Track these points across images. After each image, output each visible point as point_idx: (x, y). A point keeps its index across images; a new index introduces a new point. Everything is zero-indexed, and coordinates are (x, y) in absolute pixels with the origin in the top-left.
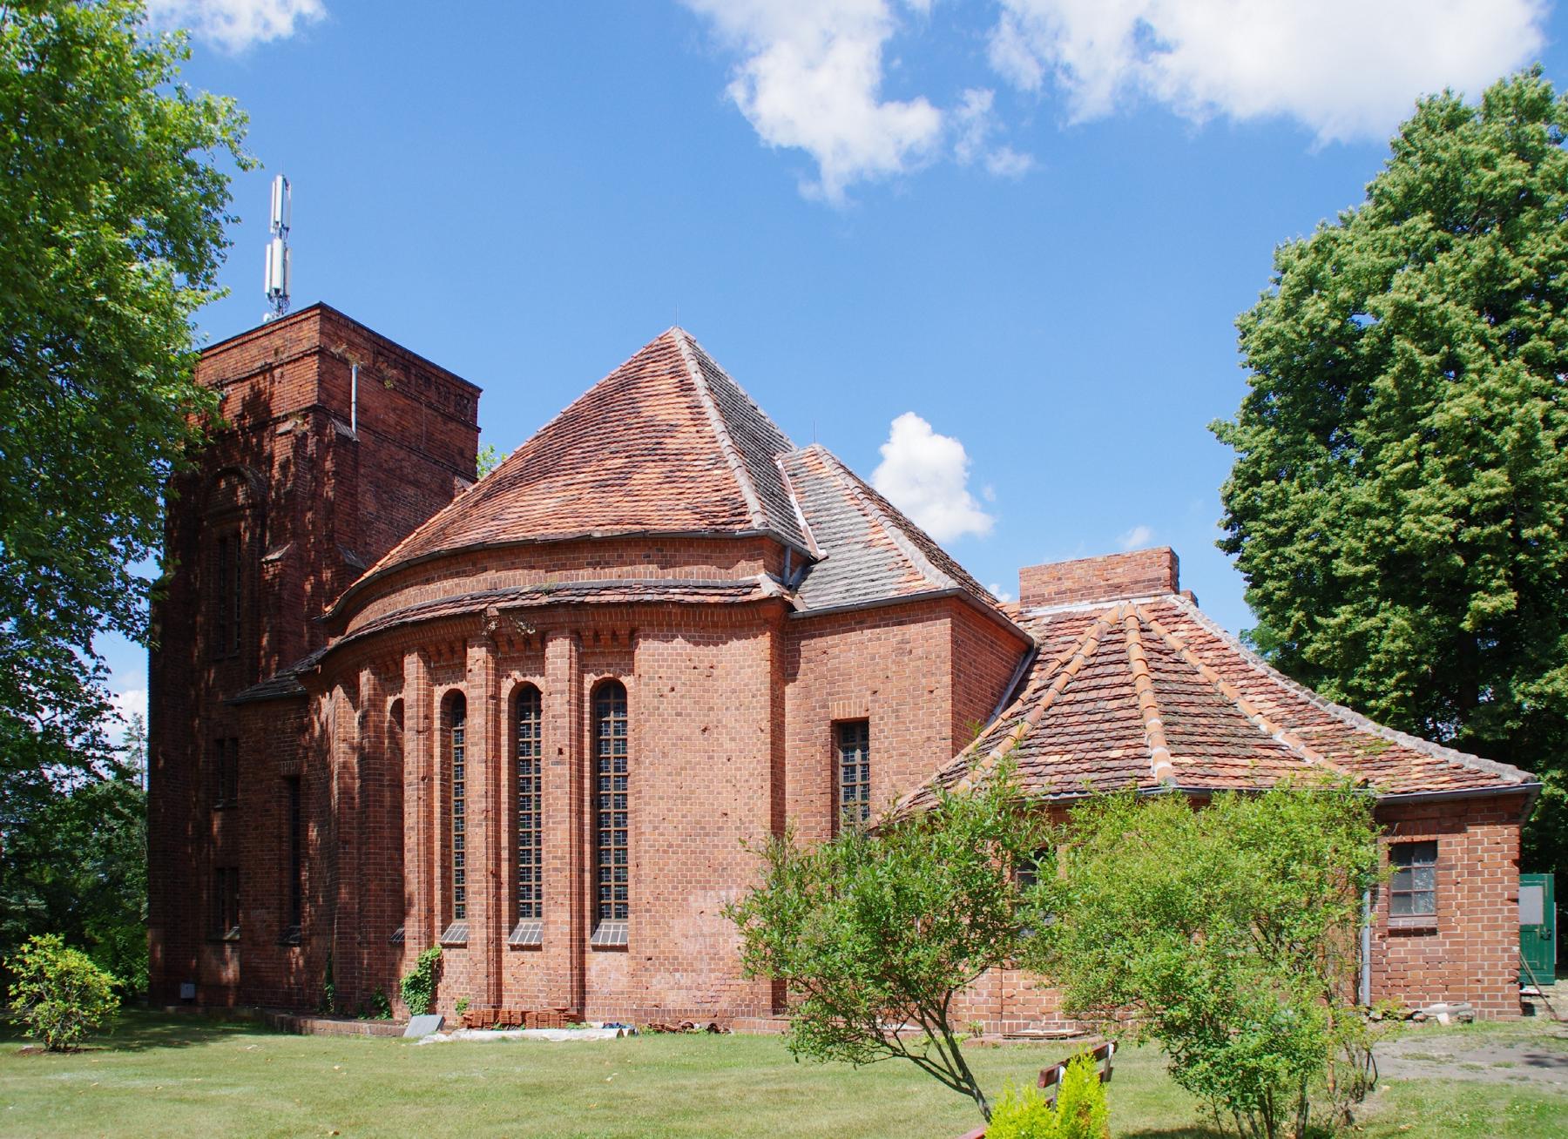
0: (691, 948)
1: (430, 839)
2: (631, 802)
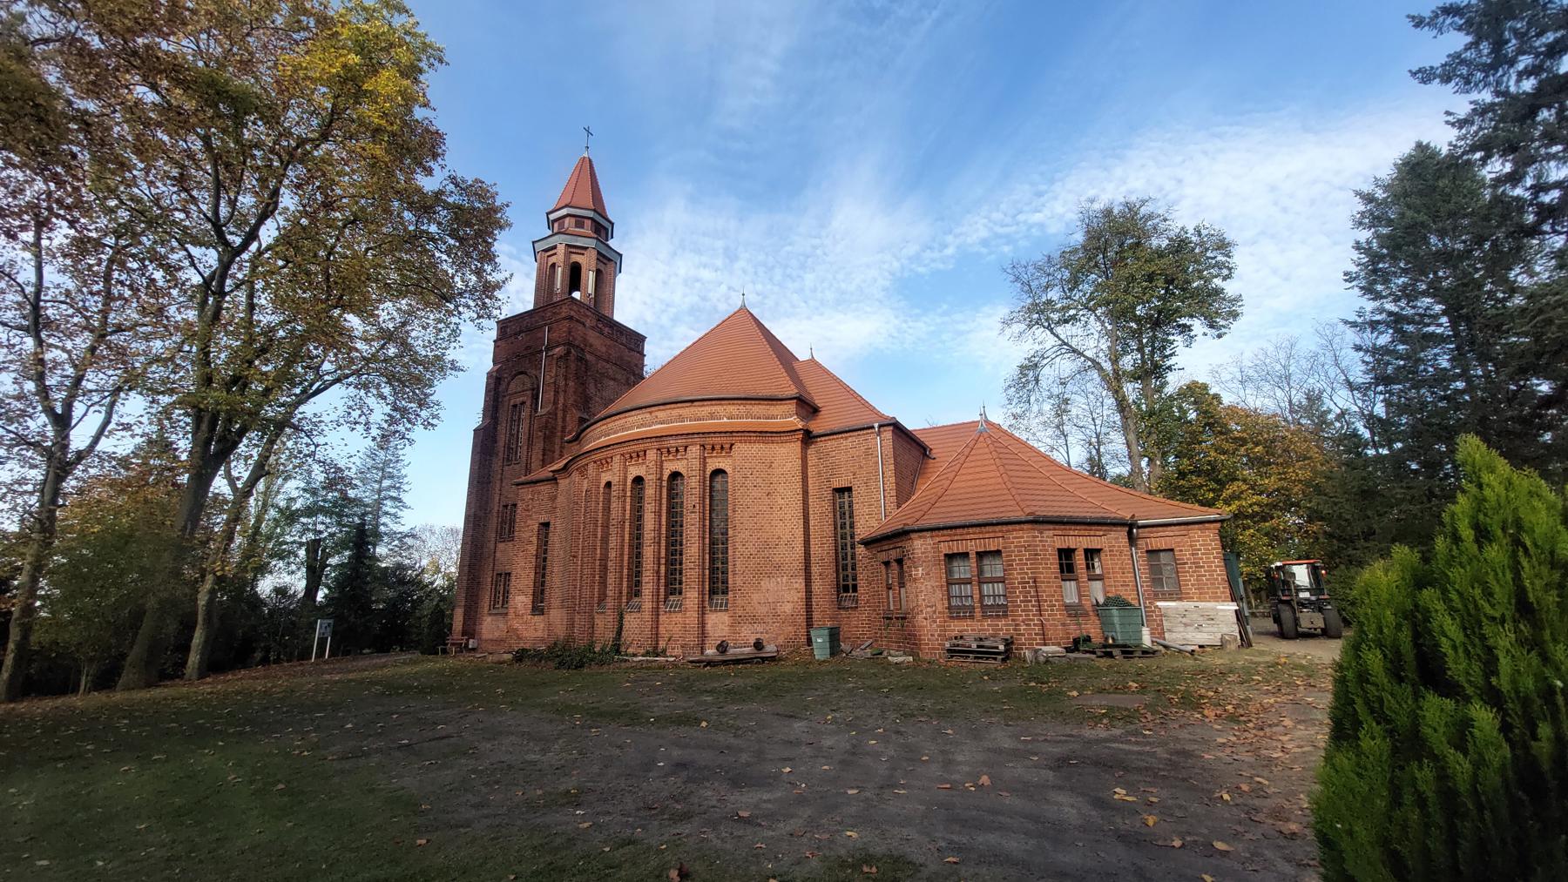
0: (763, 610)
2: (730, 532)
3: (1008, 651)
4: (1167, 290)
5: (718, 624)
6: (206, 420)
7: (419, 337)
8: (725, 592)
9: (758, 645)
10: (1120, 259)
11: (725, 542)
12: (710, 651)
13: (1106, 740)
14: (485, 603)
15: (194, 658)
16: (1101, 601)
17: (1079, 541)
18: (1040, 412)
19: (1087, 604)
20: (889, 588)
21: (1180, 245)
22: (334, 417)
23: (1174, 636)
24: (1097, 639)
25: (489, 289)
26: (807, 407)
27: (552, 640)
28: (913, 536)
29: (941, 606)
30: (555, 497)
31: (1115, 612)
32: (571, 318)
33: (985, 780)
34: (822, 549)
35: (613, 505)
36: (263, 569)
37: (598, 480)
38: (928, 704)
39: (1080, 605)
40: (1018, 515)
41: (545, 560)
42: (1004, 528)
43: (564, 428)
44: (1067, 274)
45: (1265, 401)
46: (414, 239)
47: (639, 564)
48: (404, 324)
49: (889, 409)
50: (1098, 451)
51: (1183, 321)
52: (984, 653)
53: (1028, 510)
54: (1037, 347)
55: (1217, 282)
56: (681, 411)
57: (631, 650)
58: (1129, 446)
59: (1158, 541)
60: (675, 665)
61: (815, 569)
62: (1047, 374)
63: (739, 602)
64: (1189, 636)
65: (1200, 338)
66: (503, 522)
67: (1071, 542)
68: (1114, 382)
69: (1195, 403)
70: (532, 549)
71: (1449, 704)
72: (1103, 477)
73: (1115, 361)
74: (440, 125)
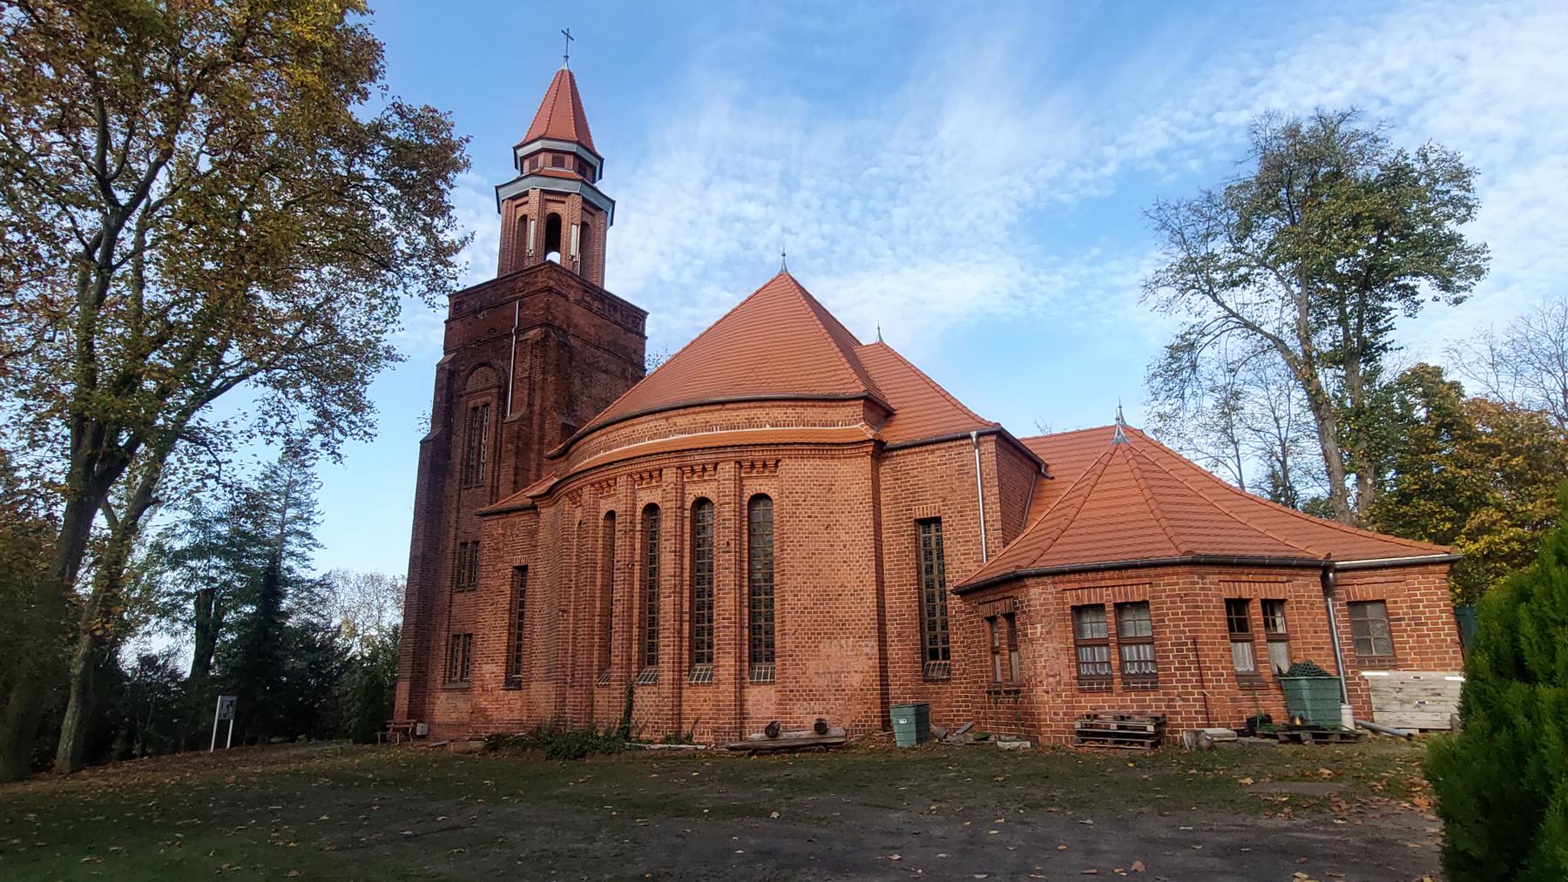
0: (822, 682)
1: (631, 608)
2: (777, 578)
3: (1159, 733)
4: (1380, 237)
5: (762, 701)
6: (89, 431)
7: (349, 319)
8: (770, 658)
9: (821, 727)
10: (1310, 199)
11: (770, 592)
12: (756, 736)
13: (1286, 829)
14: (438, 674)
15: (65, 745)
16: (1285, 669)
17: (1255, 589)
18: (1199, 411)
19: (1266, 673)
20: (995, 651)
21: (1398, 175)
22: (244, 425)
23: (1386, 716)
24: (1279, 719)
25: (443, 253)
26: (878, 410)
27: (533, 724)
28: (1029, 582)
29: (1067, 676)
30: (536, 532)
31: (1304, 682)
32: (550, 290)
33: (1138, 865)
34: (903, 602)
35: (618, 543)
36: (127, 629)
37: (597, 510)
38: (1058, 793)
39: (1256, 674)
40: (1173, 554)
41: (521, 616)
42: (1152, 572)
43: (542, 438)
44: (1235, 219)
45: (1528, 392)
46: (342, 189)
47: (653, 621)
48: (328, 299)
49: (991, 410)
50: (1283, 464)
51: (1408, 280)
52: (1126, 736)
53: (1184, 548)
54: (1196, 321)
55: (1451, 226)
56: (708, 416)
57: (644, 736)
58: (1327, 459)
59: (1364, 589)
60: (708, 754)
61: (892, 628)
62: (1208, 356)
63: (790, 672)
64: (1406, 717)
65: (1428, 305)
66: (461, 565)
67: (1244, 591)
68: (1304, 368)
69: (1424, 395)
70: (504, 602)
71: (1525, 687)
72: (1291, 501)
73: (1306, 340)
74: (377, 33)
